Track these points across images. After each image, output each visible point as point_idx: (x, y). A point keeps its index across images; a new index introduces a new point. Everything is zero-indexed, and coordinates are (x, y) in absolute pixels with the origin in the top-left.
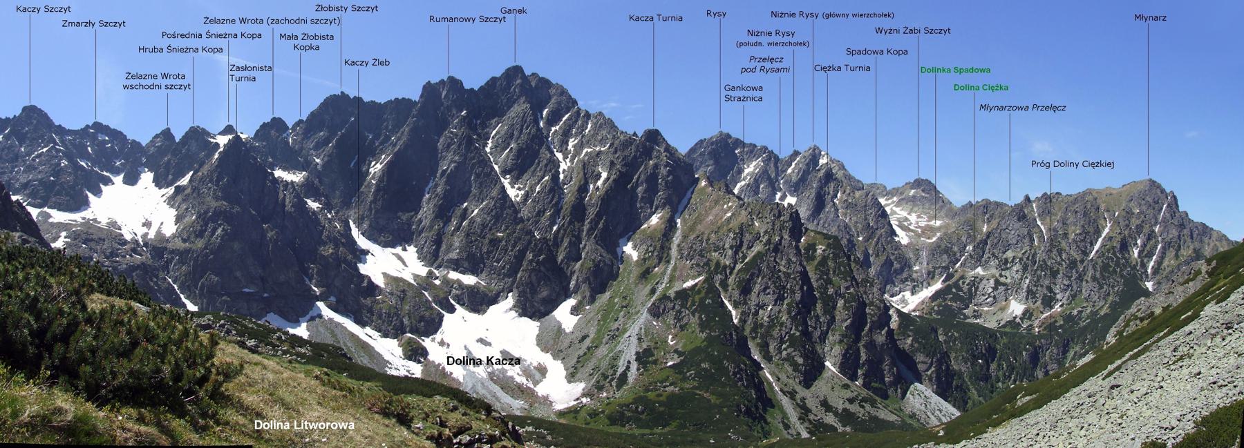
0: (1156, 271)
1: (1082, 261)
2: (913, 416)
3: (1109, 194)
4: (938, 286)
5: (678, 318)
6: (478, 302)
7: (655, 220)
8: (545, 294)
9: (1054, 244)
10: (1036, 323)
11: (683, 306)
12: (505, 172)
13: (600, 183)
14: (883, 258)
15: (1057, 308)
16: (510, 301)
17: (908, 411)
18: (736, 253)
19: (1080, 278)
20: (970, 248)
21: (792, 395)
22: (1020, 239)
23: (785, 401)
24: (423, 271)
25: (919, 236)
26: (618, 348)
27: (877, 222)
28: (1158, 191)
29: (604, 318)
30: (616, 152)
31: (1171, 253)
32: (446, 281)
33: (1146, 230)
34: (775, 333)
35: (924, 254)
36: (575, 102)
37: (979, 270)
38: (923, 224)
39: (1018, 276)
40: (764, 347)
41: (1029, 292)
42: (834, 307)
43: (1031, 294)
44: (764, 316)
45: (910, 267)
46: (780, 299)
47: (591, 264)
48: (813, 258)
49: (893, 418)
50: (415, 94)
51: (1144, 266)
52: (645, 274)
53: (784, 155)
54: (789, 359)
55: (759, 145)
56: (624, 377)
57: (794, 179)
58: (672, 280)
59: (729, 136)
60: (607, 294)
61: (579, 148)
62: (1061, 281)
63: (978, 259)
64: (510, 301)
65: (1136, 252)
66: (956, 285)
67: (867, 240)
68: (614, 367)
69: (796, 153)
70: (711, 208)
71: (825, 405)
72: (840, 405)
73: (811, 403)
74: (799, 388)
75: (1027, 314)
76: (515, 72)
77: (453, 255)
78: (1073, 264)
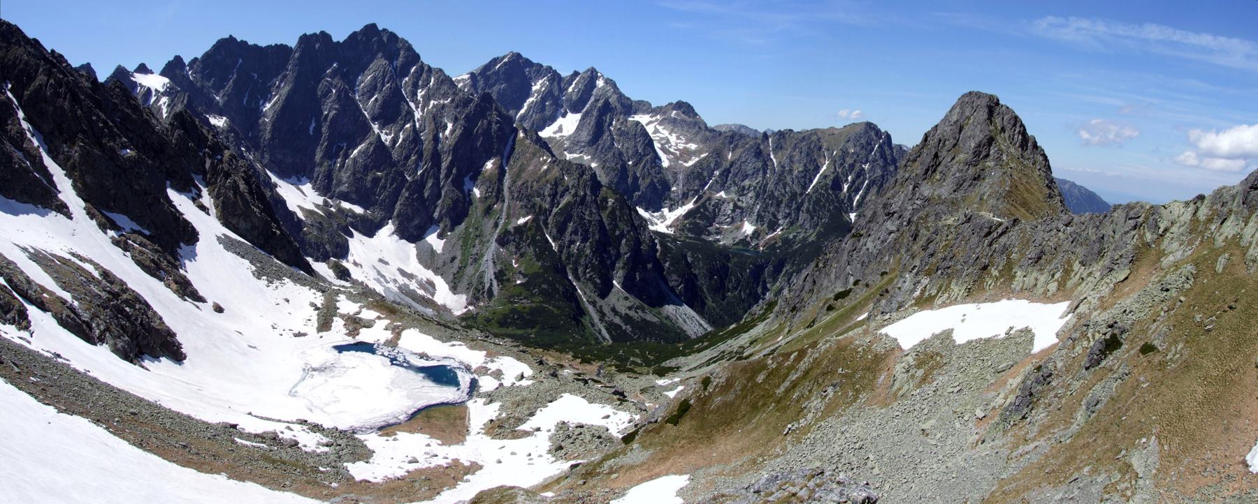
0: (860, 204)
1: (801, 194)
2: (668, 318)
3: (831, 132)
4: (690, 206)
5: (518, 248)
6: (370, 229)
7: (489, 165)
8: (416, 222)
9: (781, 179)
10: (762, 242)
11: (521, 239)
12: (374, 119)
13: (447, 132)
14: (648, 181)
15: (779, 231)
16: (389, 227)
17: (664, 314)
18: (553, 201)
19: (798, 209)
20: (717, 173)
21: (594, 303)
22: (756, 172)
23: (590, 308)
24: (320, 200)
25: (677, 159)
26: (482, 269)
27: (644, 150)
28: (873, 134)
29: (465, 244)
30: (457, 107)
31: (874, 190)
32: (341, 210)
33: (857, 169)
34: (582, 261)
35: (681, 177)
36: (417, 57)
37: (722, 194)
38: (681, 146)
39: (751, 202)
40: (575, 272)
41: (759, 215)
42: (620, 244)
43: (760, 218)
44: (574, 249)
45: (669, 189)
46: (584, 240)
47: (450, 202)
48: (606, 208)
49: (655, 320)
50: (292, 43)
51: (851, 200)
52: (488, 211)
53: (565, 73)
54: (591, 279)
55: (545, 64)
56: (490, 290)
57: (574, 98)
58: (508, 216)
59: (519, 56)
60: (463, 225)
61: (427, 98)
62: (784, 210)
63: (722, 185)
64: (389, 227)
65: (846, 187)
66: (704, 205)
67: (635, 164)
68: (482, 283)
69: (576, 74)
70: (531, 159)
71: (613, 310)
72: (623, 311)
73: (606, 310)
74: (597, 299)
75: (756, 234)
76: (371, 29)
77: (344, 188)
78: (794, 196)
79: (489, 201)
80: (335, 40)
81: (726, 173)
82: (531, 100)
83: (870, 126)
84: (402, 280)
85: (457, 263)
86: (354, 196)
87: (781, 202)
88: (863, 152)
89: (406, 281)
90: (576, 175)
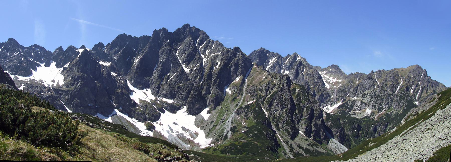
0: (419, 98)
1: (392, 94)
2: (331, 150)
3: (402, 70)
4: (340, 103)
5: (246, 115)
6: (173, 109)
7: (237, 79)
10: (376, 117)
11: (248, 111)
12: (183, 62)
13: (217, 66)
15: (383, 111)
16: (185, 109)
17: (329, 149)
18: (267, 91)
19: (392, 101)
20: (352, 90)
21: (287, 143)
22: (370, 87)
23: (285, 145)
24: (153, 98)
25: (333, 85)
26: (224, 126)
27: (318, 80)
28: (420, 69)
29: (219, 115)
31: (425, 92)
32: (162, 102)
33: (416, 83)
34: (281, 120)
35: (335, 92)
36: (208, 37)
37: (355, 98)
38: (335, 81)
39: (369, 100)
40: (277, 126)
41: (373, 105)
42: (303, 111)
43: (374, 106)
44: (277, 114)
45: (330, 97)
46: (283, 108)
48: (295, 93)
49: (324, 151)
50: (150, 34)
51: (415, 96)
52: (234, 99)
53: (284, 56)
54: (286, 130)
55: (275, 52)
56: (226, 136)
58: (243, 101)
59: (264, 49)
60: (220, 106)
61: (210, 53)
62: (385, 102)
63: (355, 94)
64: (185, 109)
65: (412, 91)
66: (347, 103)
67: (314, 87)
68: (222, 133)
69: (289, 55)
70: (258, 75)
71: (299, 146)
72: (304, 146)
73: (294, 146)
74: (290, 140)
75: (373, 114)
76: (187, 26)
77: (164, 92)
78: (389, 95)
79: (235, 95)
80: (169, 31)
81: (356, 89)
82: (269, 66)
83: (418, 66)
84: (181, 131)
85: (213, 124)
86: (169, 96)
87: (383, 98)
88: (417, 77)
89: (184, 132)
90: (279, 79)
